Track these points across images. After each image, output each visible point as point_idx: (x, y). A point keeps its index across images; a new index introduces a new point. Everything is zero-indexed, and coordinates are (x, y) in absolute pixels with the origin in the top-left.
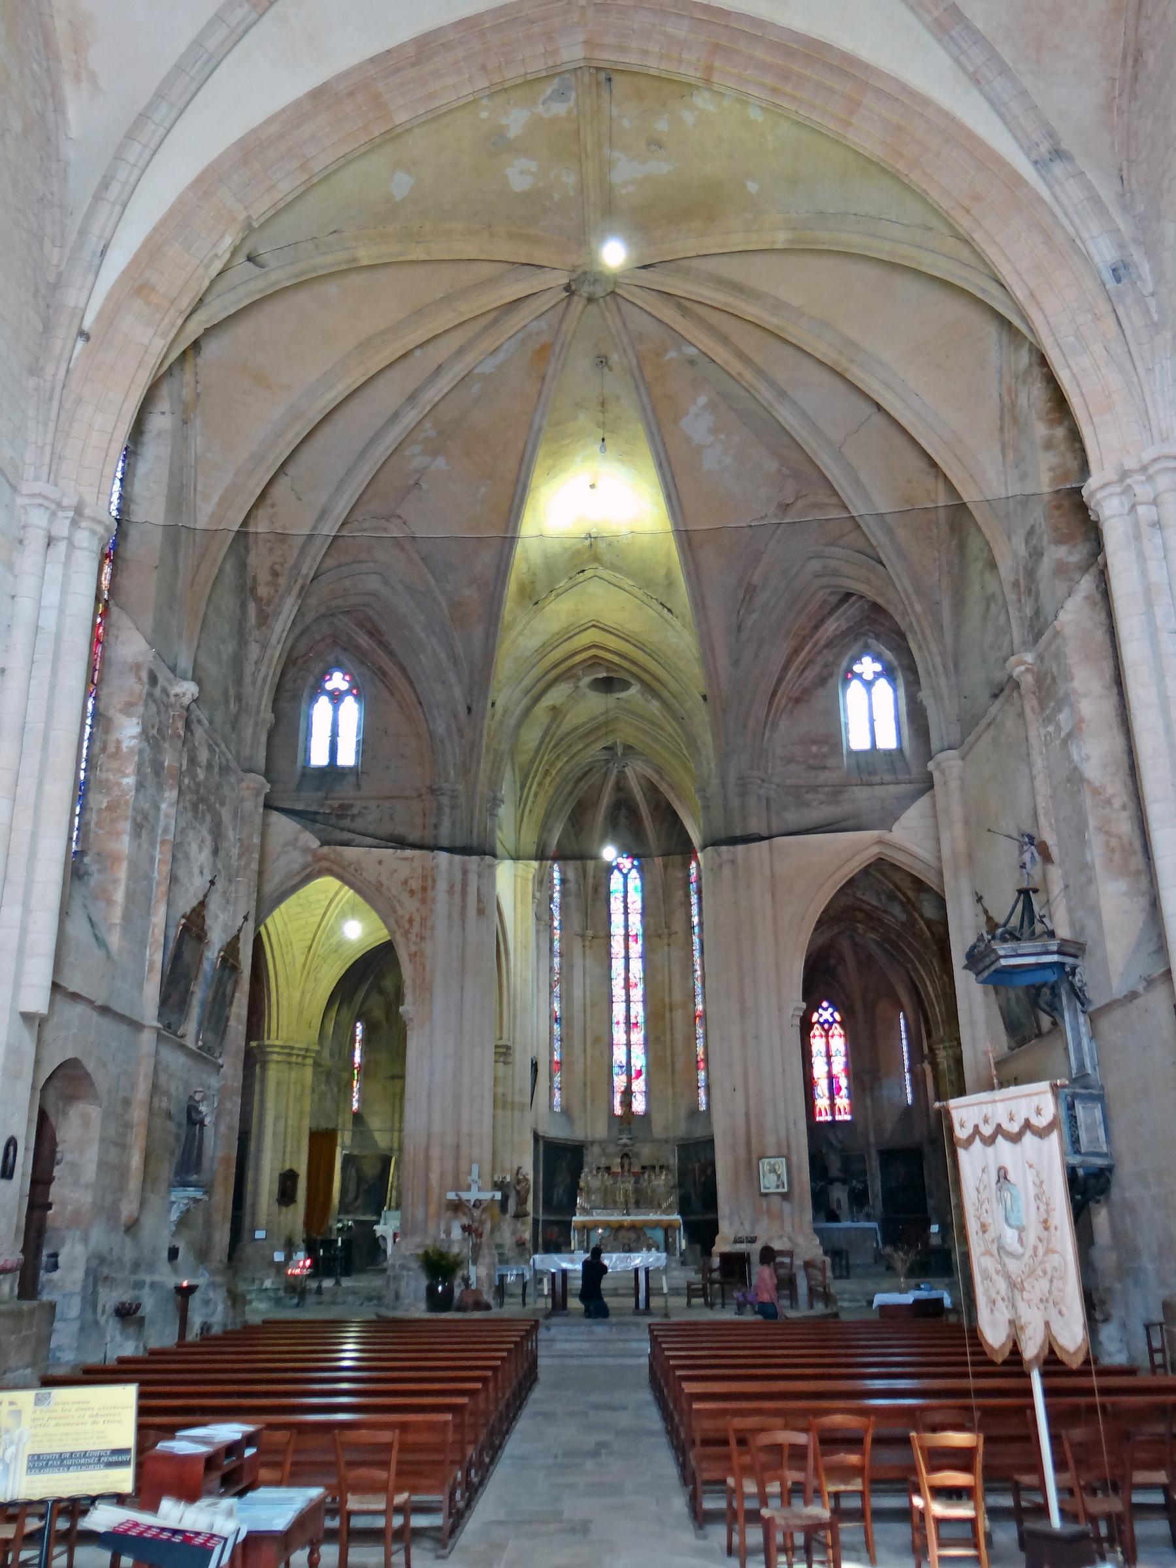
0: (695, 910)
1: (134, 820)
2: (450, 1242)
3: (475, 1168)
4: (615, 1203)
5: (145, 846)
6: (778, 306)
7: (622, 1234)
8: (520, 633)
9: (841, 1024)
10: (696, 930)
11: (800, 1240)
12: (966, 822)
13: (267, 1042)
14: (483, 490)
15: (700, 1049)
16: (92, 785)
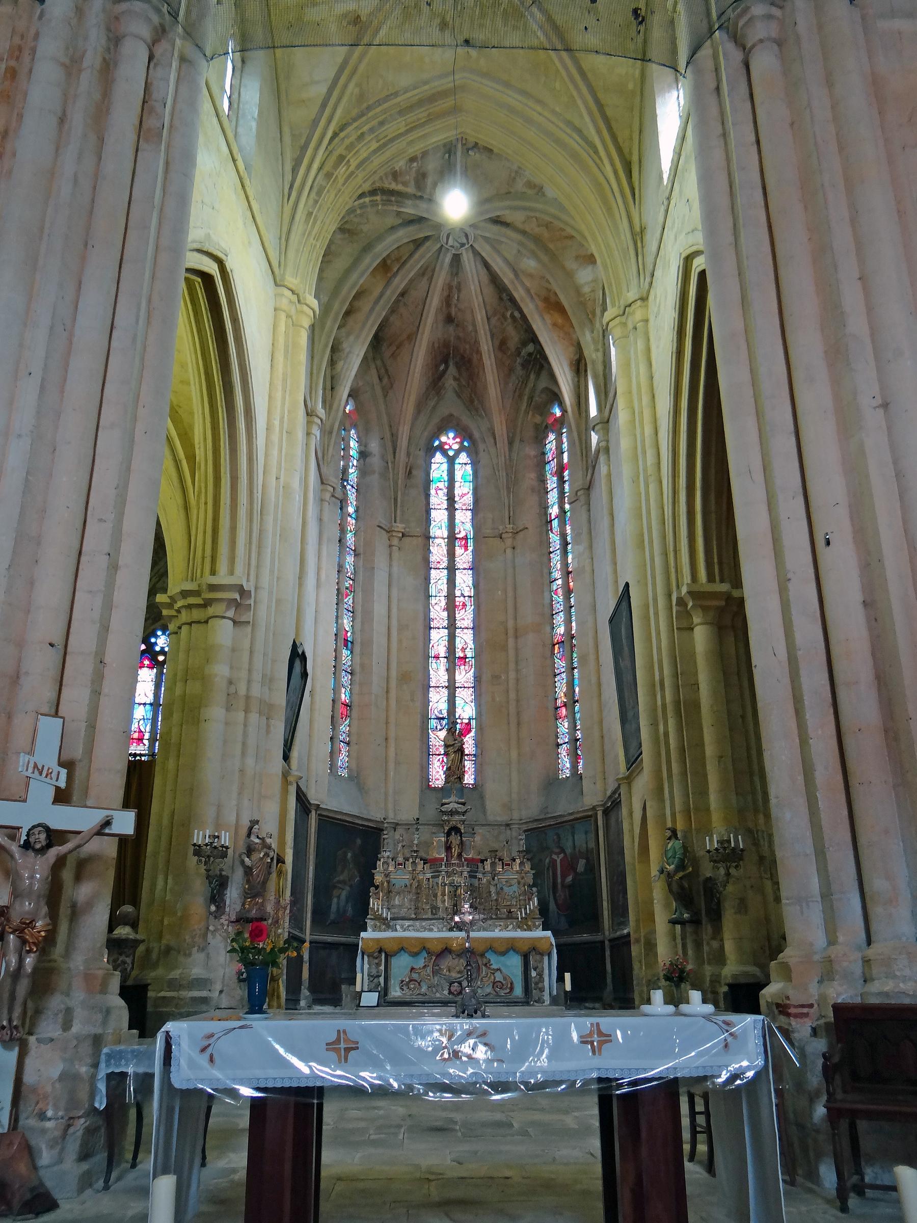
0: (553, 497)
4: (435, 909)
7: (447, 962)
10: (555, 523)
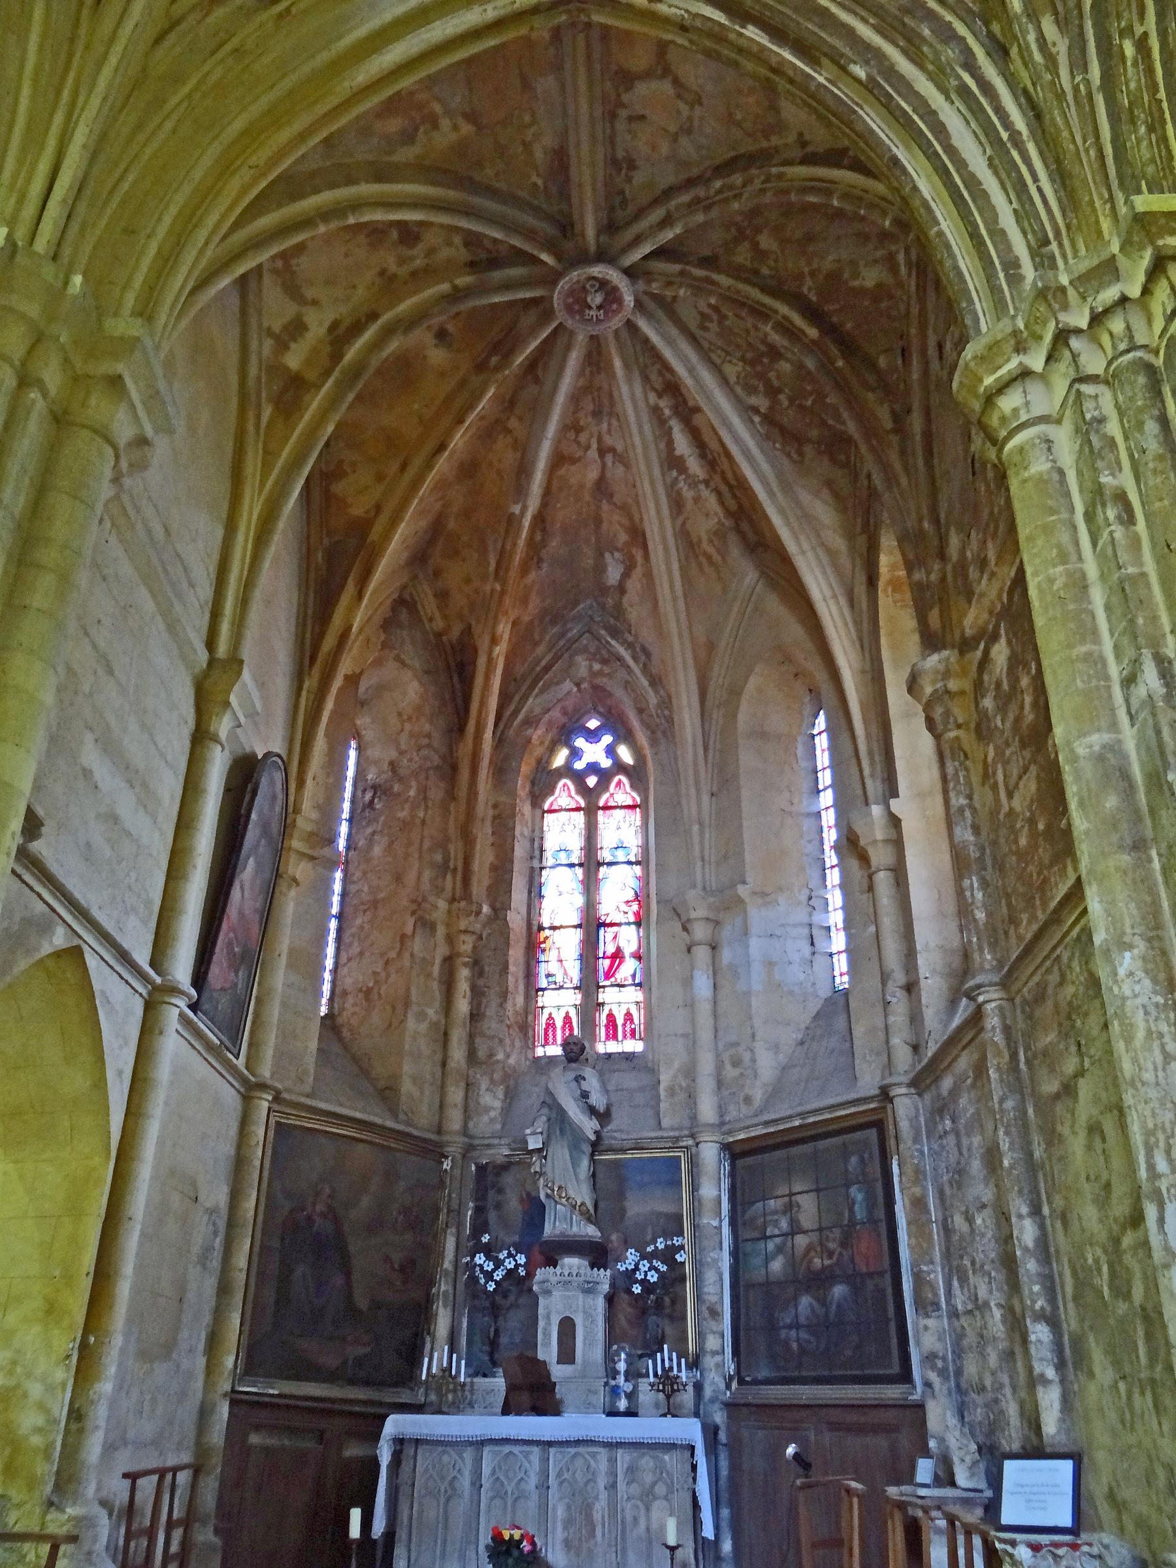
9: (636, 775)
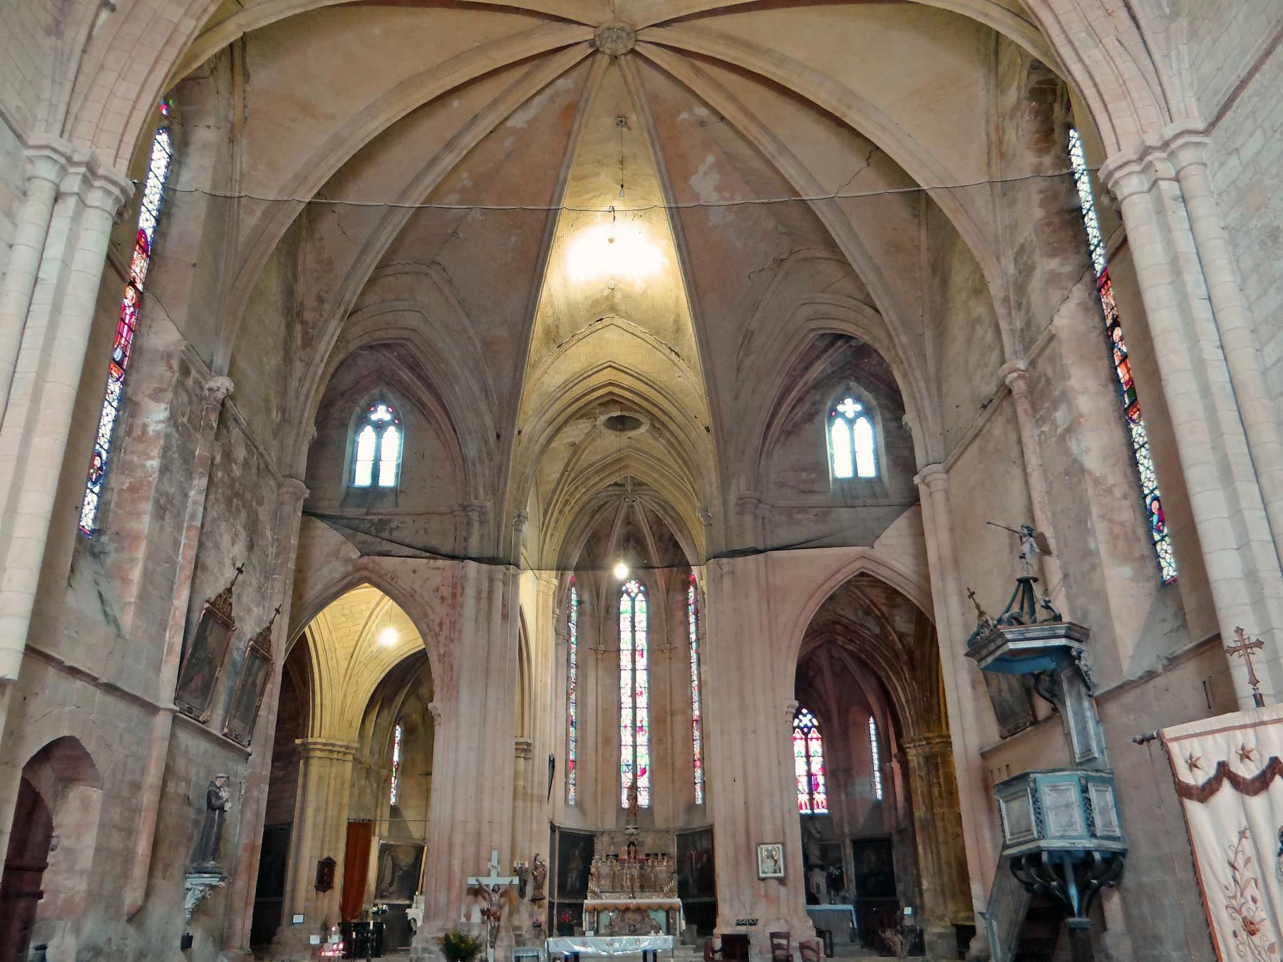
0: (693, 628)
1: (157, 501)
2: (469, 925)
3: (495, 854)
4: (622, 886)
5: (169, 529)
6: (782, 61)
7: (629, 915)
8: (546, 372)
10: (694, 645)
11: (795, 922)
12: (952, 529)
13: (310, 740)
14: (513, 239)
15: (697, 749)
16: (114, 466)
